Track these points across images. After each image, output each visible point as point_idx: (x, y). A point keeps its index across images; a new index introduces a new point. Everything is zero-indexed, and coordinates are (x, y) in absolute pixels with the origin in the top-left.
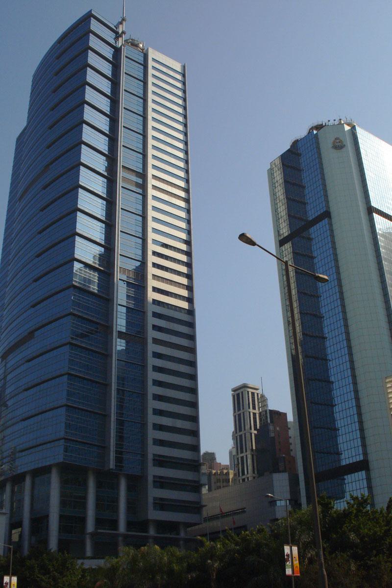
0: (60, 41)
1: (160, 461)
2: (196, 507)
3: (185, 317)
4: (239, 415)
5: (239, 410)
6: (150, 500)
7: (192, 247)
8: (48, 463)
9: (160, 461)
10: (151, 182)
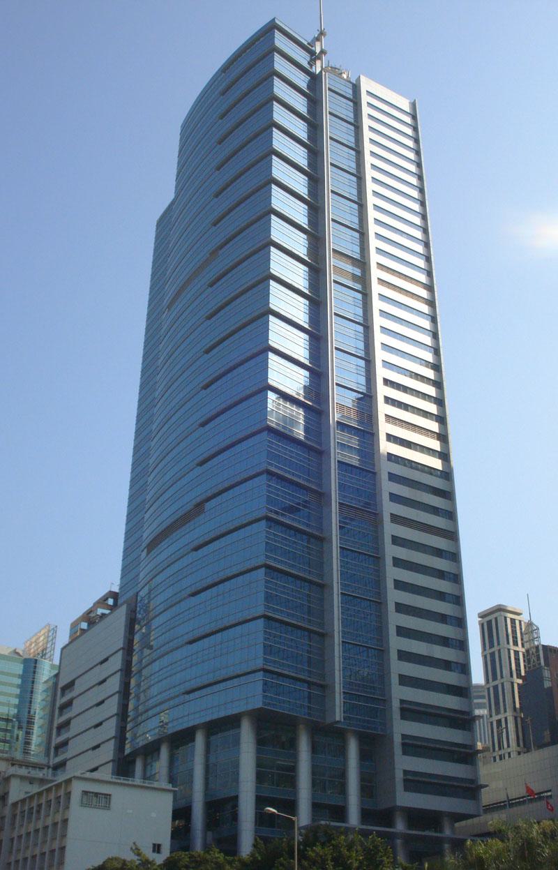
0: (225, 69)
1: (411, 712)
2: (471, 789)
3: (438, 483)
4: (492, 654)
5: (492, 646)
6: (399, 775)
7: (443, 373)
8: (235, 711)
9: (411, 712)
10: (375, 273)
